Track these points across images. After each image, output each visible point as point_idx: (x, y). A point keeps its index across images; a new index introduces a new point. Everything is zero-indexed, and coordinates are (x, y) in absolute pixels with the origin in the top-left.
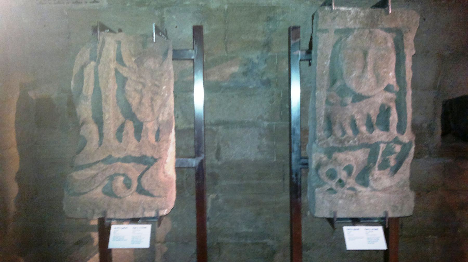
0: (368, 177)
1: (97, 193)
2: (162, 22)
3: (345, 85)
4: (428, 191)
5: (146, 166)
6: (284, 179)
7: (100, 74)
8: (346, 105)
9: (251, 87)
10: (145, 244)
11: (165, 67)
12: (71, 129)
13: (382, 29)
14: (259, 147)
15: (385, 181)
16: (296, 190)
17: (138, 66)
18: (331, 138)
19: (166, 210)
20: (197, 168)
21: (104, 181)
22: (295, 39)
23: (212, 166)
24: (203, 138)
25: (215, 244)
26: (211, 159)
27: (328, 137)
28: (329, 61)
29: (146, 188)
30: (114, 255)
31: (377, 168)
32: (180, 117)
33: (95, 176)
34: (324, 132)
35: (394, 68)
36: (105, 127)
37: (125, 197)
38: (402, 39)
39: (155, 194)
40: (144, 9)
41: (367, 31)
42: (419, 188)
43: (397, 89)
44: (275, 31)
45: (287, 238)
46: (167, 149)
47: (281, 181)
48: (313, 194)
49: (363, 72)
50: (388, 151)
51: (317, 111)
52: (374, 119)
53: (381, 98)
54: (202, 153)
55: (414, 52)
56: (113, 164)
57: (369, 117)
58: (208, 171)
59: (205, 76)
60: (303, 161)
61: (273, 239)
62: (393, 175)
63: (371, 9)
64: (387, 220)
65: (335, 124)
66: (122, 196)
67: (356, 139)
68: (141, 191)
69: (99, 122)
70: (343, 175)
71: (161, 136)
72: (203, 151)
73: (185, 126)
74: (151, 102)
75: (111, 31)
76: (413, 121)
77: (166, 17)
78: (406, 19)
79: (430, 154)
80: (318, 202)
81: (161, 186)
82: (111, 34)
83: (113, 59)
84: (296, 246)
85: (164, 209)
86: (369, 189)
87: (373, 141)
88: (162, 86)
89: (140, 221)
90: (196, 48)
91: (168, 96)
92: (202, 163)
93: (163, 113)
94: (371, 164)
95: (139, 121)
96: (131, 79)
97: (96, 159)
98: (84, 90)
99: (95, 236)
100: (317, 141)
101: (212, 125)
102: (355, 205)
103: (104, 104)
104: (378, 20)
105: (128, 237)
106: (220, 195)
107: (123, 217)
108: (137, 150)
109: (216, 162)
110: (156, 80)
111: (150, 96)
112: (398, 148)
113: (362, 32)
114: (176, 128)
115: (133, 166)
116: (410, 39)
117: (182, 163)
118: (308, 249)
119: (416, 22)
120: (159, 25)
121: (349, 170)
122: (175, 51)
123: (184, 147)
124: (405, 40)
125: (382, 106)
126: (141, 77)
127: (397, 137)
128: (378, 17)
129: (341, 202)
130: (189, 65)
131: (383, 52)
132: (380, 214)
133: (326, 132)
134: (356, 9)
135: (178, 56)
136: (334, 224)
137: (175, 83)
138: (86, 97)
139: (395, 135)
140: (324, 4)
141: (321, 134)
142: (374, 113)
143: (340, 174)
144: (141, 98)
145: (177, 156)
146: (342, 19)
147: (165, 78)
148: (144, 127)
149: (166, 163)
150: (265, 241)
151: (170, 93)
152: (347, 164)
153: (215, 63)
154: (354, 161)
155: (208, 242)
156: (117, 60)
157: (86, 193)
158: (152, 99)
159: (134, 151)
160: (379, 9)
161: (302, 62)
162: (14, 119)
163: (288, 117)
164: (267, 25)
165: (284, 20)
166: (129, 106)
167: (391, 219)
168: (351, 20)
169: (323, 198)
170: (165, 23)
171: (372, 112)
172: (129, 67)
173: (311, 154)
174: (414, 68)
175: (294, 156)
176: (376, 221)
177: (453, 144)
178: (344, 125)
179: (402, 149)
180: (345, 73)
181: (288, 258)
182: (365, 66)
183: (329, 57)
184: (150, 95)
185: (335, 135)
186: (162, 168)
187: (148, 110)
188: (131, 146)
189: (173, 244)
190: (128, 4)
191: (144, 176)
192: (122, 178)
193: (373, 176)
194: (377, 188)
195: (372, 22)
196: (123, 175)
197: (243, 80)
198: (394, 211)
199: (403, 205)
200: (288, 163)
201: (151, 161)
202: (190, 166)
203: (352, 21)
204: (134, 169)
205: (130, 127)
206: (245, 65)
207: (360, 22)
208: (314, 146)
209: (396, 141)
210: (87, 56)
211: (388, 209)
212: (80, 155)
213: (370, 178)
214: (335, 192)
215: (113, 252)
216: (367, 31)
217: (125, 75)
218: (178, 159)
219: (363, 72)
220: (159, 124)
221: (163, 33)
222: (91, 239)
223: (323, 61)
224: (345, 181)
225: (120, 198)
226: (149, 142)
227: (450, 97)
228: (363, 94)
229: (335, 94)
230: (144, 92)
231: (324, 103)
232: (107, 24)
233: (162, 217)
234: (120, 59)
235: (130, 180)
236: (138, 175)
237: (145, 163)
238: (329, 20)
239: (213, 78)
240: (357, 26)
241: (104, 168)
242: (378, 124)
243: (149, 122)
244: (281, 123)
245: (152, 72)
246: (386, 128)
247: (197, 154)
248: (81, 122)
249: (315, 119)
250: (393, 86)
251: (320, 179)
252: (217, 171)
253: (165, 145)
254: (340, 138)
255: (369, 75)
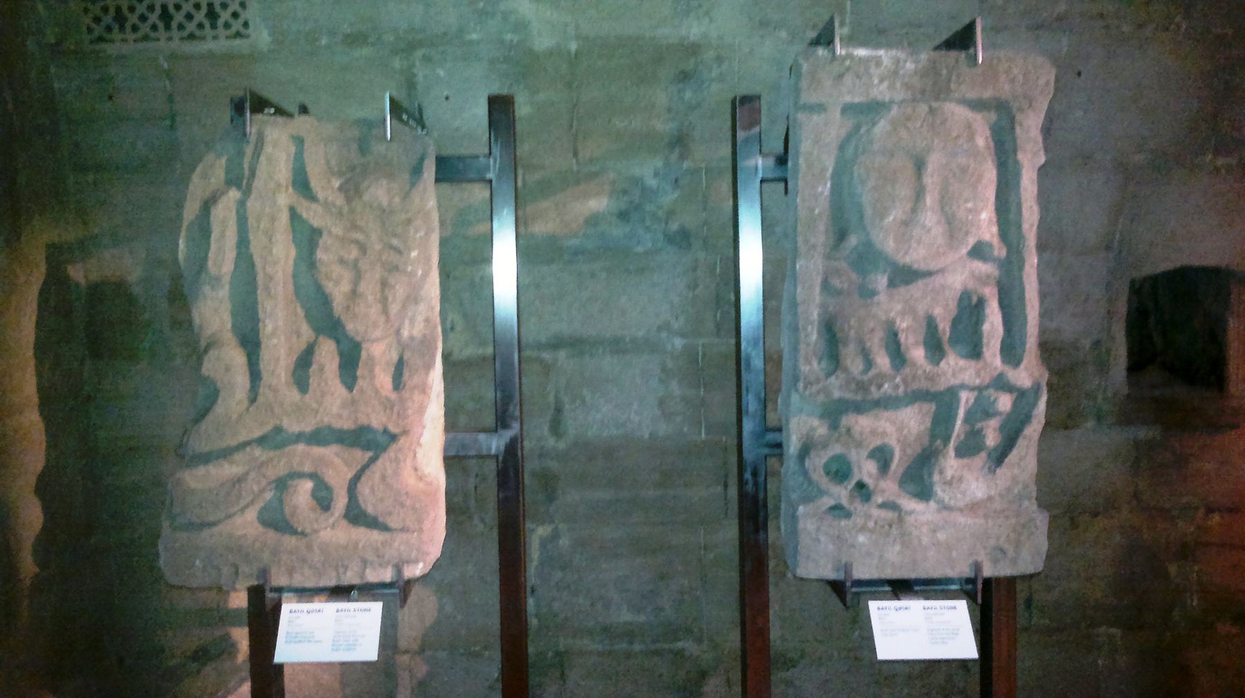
0: (930, 475)
1: (246, 524)
2: (411, 85)
3: (868, 245)
4: (1095, 515)
5: (370, 454)
6: (726, 486)
7: (251, 221)
8: (873, 293)
9: (640, 249)
10: (368, 650)
11: (417, 200)
12: (178, 361)
13: (964, 102)
14: (661, 403)
15: (974, 485)
16: (754, 513)
17: (349, 200)
18: (837, 378)
19: (421, 565)
20: (501, 458)
21: (262, 491)
22: (750, 126)
23: (542, 455)
24: (517, 381)
25: (550, 654)
26: (537, 436)
27: (829, 375)
28: (829, 185)
29: (370, 510)
30: (289, 684)
31: (952, 453)
32: (458, 328)
33: (240, 480)
34: (819, 363)
35: (992, 198)
36: (265, 355)
37: (316, 531)
38: (1013, 128)
39: (392, 525)
40: (366, 51)
41: (923, 108)
42: (1067, 509)
43: (1000, 251)
44: (699, 105)
45: (733, 639)
46: (421, 410)
47: (720, 489)
48: (794, 518)
49: (914, 210)
50: (982, 410)
51: (800, 309)
52: (944, 330)
53: (960, 273)
54: (516, 419)
55: (1042, 159)
56: (287, 449)
57: (931, 324)
58: (530, 466)
59: (520, 223)
60: (771, 437)
61: (699, 641)
62: (992, 471)
63: (932, 53)
64: (980, 586)
65: (845, 344)
66: (308, 530)
67: (898, 380)
68: (356, 516)
69: (251, 343)
70: (867, 470)
71: (406, 374)
72: (517, 413)
73: (471, 351)
74: (383, 291)
75: (280, 112)
76: (1043, 331)
77: (421, 73)
78: (1021, 78)
79: (1099, 419)
80: (804, 540)
81: (408, 503)
82: (280, 119)
83: (283, 182)
84: (756, 658)
85: (417, 561)
86: (933, 504)
87: (942, 385)
88: (410, 250)
89: (354, 593)
90: (496, 151)
91: (426, 274)
92: (512, 449)
93: (412, 321)
94: (939, 442)
95: (351, 340)
96: (330, 232)
97: (243, 437)
98: (210, 263)
99: (241, 637)
100: (801, 385)
101: (540, 347)
102: (898, 548)
103: (260, 292)
104: (949, 81)
105: (324, 634)
106: (561, 526)
107: (309, 584)
108: (345, 413)
109: (551, 442)
110: (395, 235)
111: (378, 276)
112: (1005, 402)
113: (909, 110)
114: (446, 357)
115: (337, 455)
116: (1030, 126)
117: (464, 446)
118: (790, 664)
119: (1047, 83)
120: (402, 97)
121: (882, 457)
122: (441, 162)
123: (470, 405)
124: (1018, 130)
125: (965, 296)
126: (355, 227)
127: (1000, 374)
128: (950, 74)
129: (861, 539)
130: (479, 193)
131: (962, 160)
132: (962, 569)
133: (824, 364)
134: (894, 52)
135: (450, 170)
136: (849, 594)
137: (443, 243)
138: (218, 279)
139: (996, 368)
140: (816, 42)
141: (812, 367)
142: (944, 315)
143: (860, 468)
144: (356, 281)
145: (451, 425)
146: (858, 77)
147: (417, 231)
148: (364, 354)
149: (419, 444)
150: (680, 645)
151: (430, 268)
152: (879, 443)
153: (546, 188)
154: (894, 436)
155: (531, 650)
156: (294, 183)
157: (214, 524)
158: (384, 284)
159: (340, 416)
160: (953, 54)
161: (765, 185)
162: (32, 338)
163: (733, 325)
164: (679, 91)
165: (721, 79)
166: (325, 301)
167: (987, 582)
168: (881, 81)
169: (818, 529)
170: (419, 87)
171: (938, 311)
172: (327, 205)
173: (787, 421)
174: (1043, 197)
175: (748, 426)
176: (954, 587)
177: (1157, 393)
178: (868, 344)
179: (1015, 404)
180: (868, 212)
181: (738, 689)
182: (919, 194)
183: (829, 174)
184: (378, 273)
185: (846, 370)
186: (409, 462)
187: (375, 311)
188: (332, 402)
189: (442, 655)
190: (324, 42)
191: (363, 479)
192: (309, 485)
193: (941, 472)
194: (952, 503)
195: (935, 83)
196: (313, 476)
197: (617, 231)
198: (995, 561)
199: (1018, 545)
200: (735, 442)
201: (382, 439)
202: (485, 452)
203: (886, 84)
204: (337, 461)
205: (327, 354)
206: (625, 192)
207: (907, 86)
208: (795, 398)
209: (1001, 383)
210: (219, 174)
211: (982, 557)
212: (203, 426)
213: (936, 477)
214: (848, 515)
215: (287, 671)
216: (923, 108)
217: (316, 223)
218: (451, 435)
219: (914, 210)
220: (403, 347)
221: (410, 116)
222: (229, 648)
223: (814, 192)
224: (871, 487)
225: (303, 534)
226: (377, 392)
227: (1148, 270)
228: (915, 266)
229: (843, 265)
230: (364, 265)
231: (818, 289)
232: (267, 93)
233: (409, 583)
234: (301, 184)
235: (328, 488)
236: (350, 476)
237: (367, 447)
238: (828, 83)
239: (539, 229)
240: (900, 95)
241: (264, 458)
242: (954, 341)
243: (377, 340)
244: (717, 340)
245: (384, 214)
246: (975, 352)
247: (502, 421)
248: (203, 344)
249: (795, 329)
250: (990, 245)
251: (810, 482)
252: (553, 465)
253: (417, 397)
254: (859, 378)
255: (930, 218)
